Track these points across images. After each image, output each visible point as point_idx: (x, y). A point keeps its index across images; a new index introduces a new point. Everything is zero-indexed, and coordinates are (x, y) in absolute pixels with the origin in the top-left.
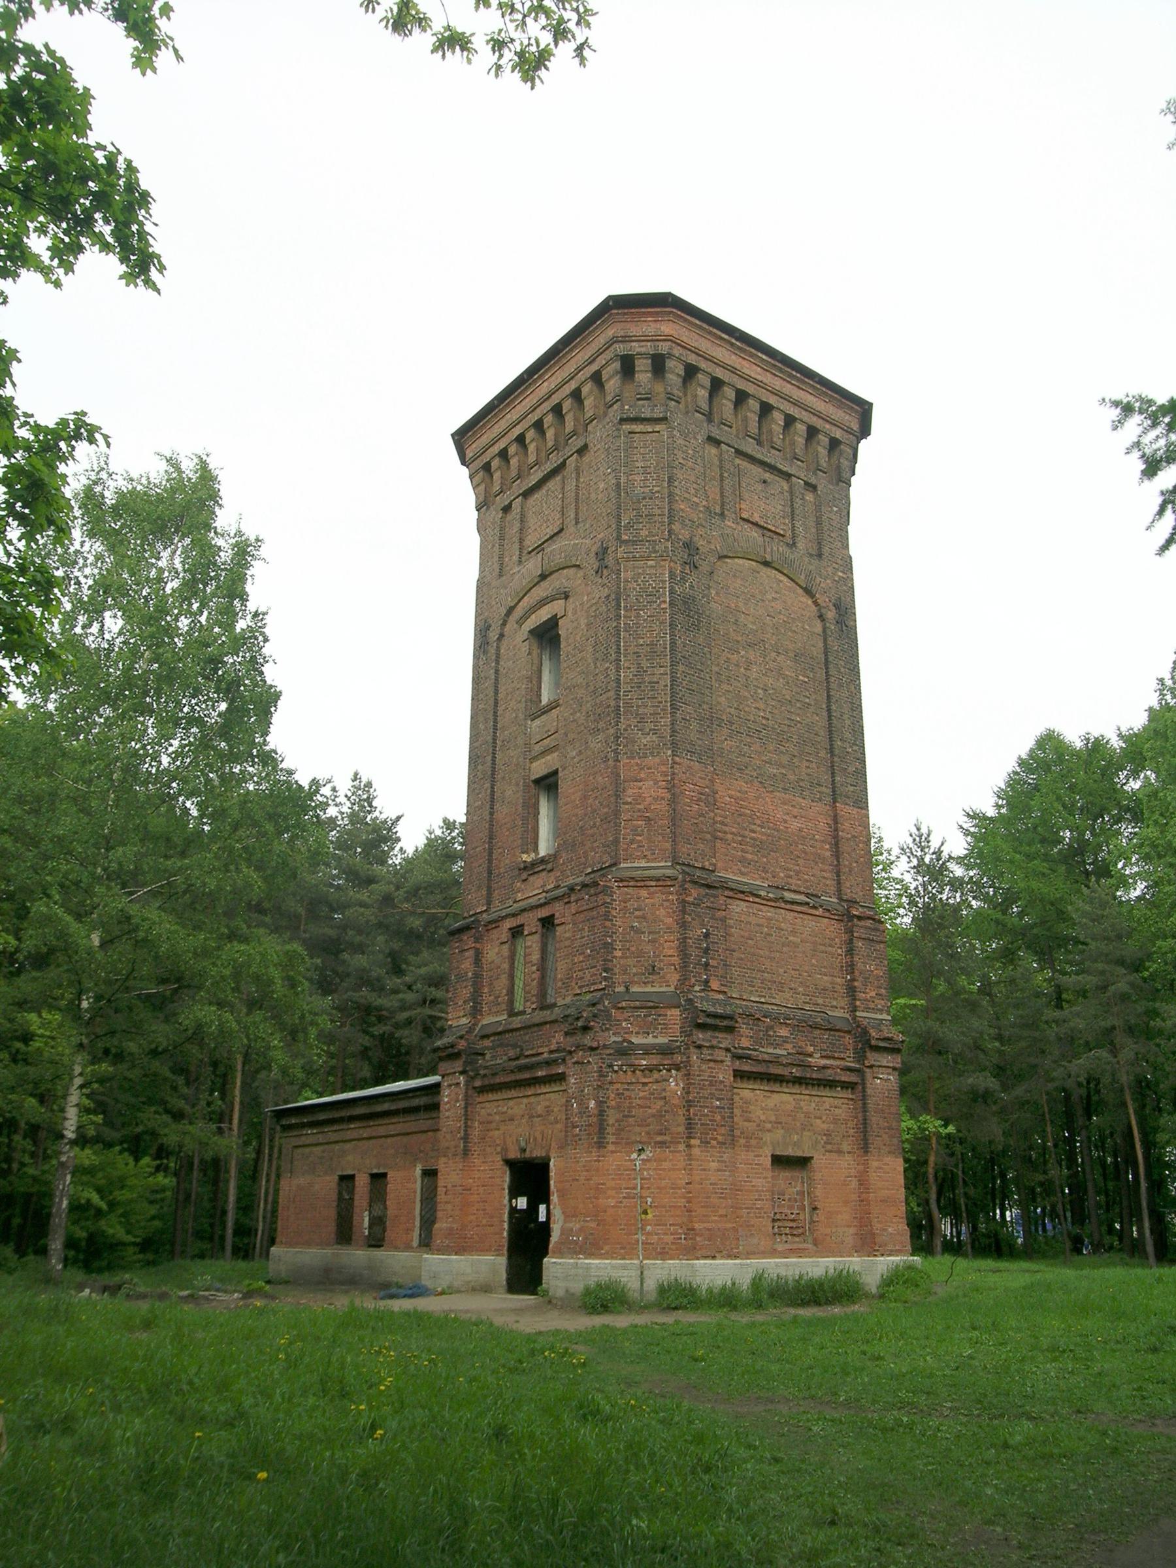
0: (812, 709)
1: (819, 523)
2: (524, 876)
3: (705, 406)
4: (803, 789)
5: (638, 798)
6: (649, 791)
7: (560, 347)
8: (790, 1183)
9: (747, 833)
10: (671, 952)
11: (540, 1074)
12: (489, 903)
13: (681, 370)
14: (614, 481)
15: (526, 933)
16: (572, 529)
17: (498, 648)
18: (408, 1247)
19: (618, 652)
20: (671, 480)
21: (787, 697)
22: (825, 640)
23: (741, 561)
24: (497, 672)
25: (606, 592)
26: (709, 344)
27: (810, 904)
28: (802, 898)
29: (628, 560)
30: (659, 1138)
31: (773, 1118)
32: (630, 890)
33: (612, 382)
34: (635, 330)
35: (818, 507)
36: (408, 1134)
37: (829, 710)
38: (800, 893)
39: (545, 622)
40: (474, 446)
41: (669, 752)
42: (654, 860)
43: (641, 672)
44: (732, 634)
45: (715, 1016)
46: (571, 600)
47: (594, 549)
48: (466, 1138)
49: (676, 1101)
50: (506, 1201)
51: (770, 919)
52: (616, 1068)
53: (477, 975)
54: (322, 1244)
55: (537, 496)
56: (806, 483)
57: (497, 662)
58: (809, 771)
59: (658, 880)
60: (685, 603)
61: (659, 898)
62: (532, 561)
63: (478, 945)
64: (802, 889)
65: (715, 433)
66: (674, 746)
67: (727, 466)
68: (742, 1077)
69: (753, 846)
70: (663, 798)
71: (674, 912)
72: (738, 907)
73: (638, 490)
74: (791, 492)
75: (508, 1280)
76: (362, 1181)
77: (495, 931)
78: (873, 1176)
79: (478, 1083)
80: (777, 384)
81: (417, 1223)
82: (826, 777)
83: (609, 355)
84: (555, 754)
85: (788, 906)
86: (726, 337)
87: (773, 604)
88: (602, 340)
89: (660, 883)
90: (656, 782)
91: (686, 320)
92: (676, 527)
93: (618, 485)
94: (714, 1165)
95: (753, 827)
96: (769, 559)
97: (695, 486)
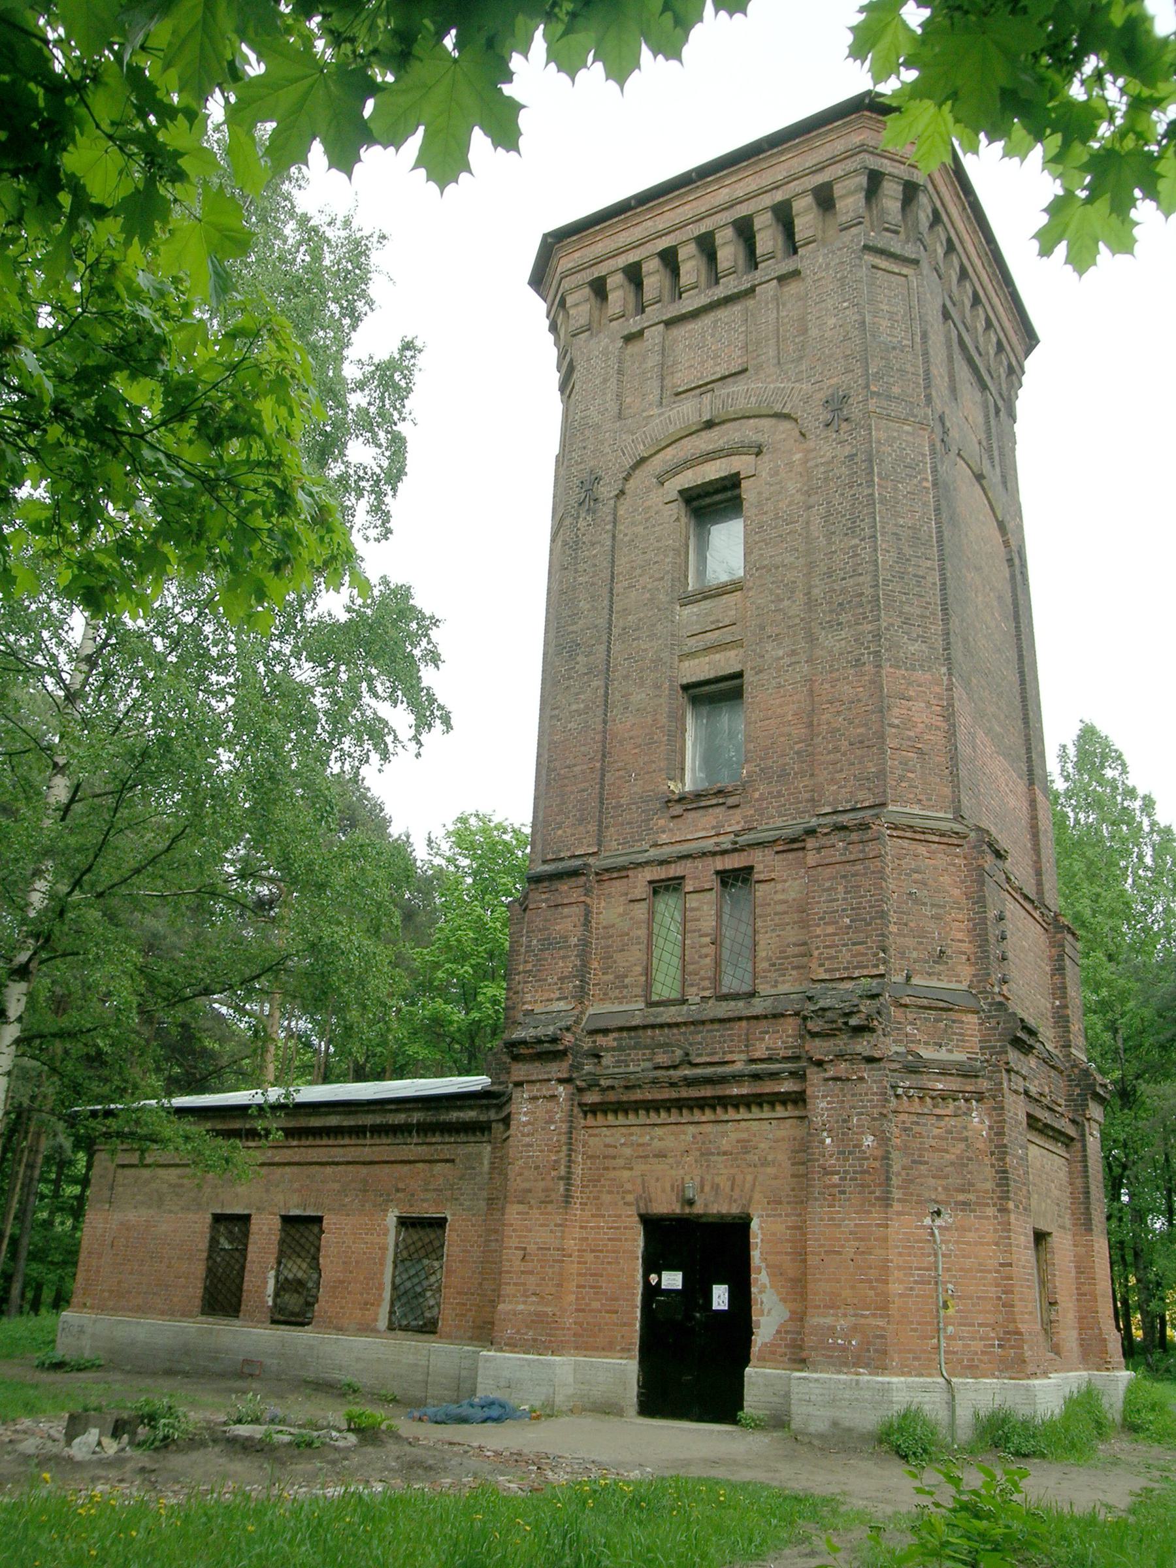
2: (677, 809)
7: (766, 146)
10: (960, 936)
11: (736, 1091)
15: (689, 888)
18: (366, 1329)
25: (847, 450)
30: (961, 1197)
32: (905, 843)
33: (850, 200)
36: (371, 1163)
39: (711, 482)
40: (577, 255)
41: (944, 670)
43: (902, 558)
46: (765, 458)
47: (821, 395)
48: (568, 1179)
49: (981, 1146)
50: (639, 1277)
52: (900, 1091)
53: (585, 943)
54: (169, 1312)
55: (691, 326)
61: (941, 860)
63: (588, 900)
70: (938, 728)
75: (640, 1395)
76: (265, 1233)
77: (617, 883)
79: (592, 1098)
81: (387, 1294)
83: (850, 165)
84: (732, 653)
88: (839, 146)
89: (945, 840)
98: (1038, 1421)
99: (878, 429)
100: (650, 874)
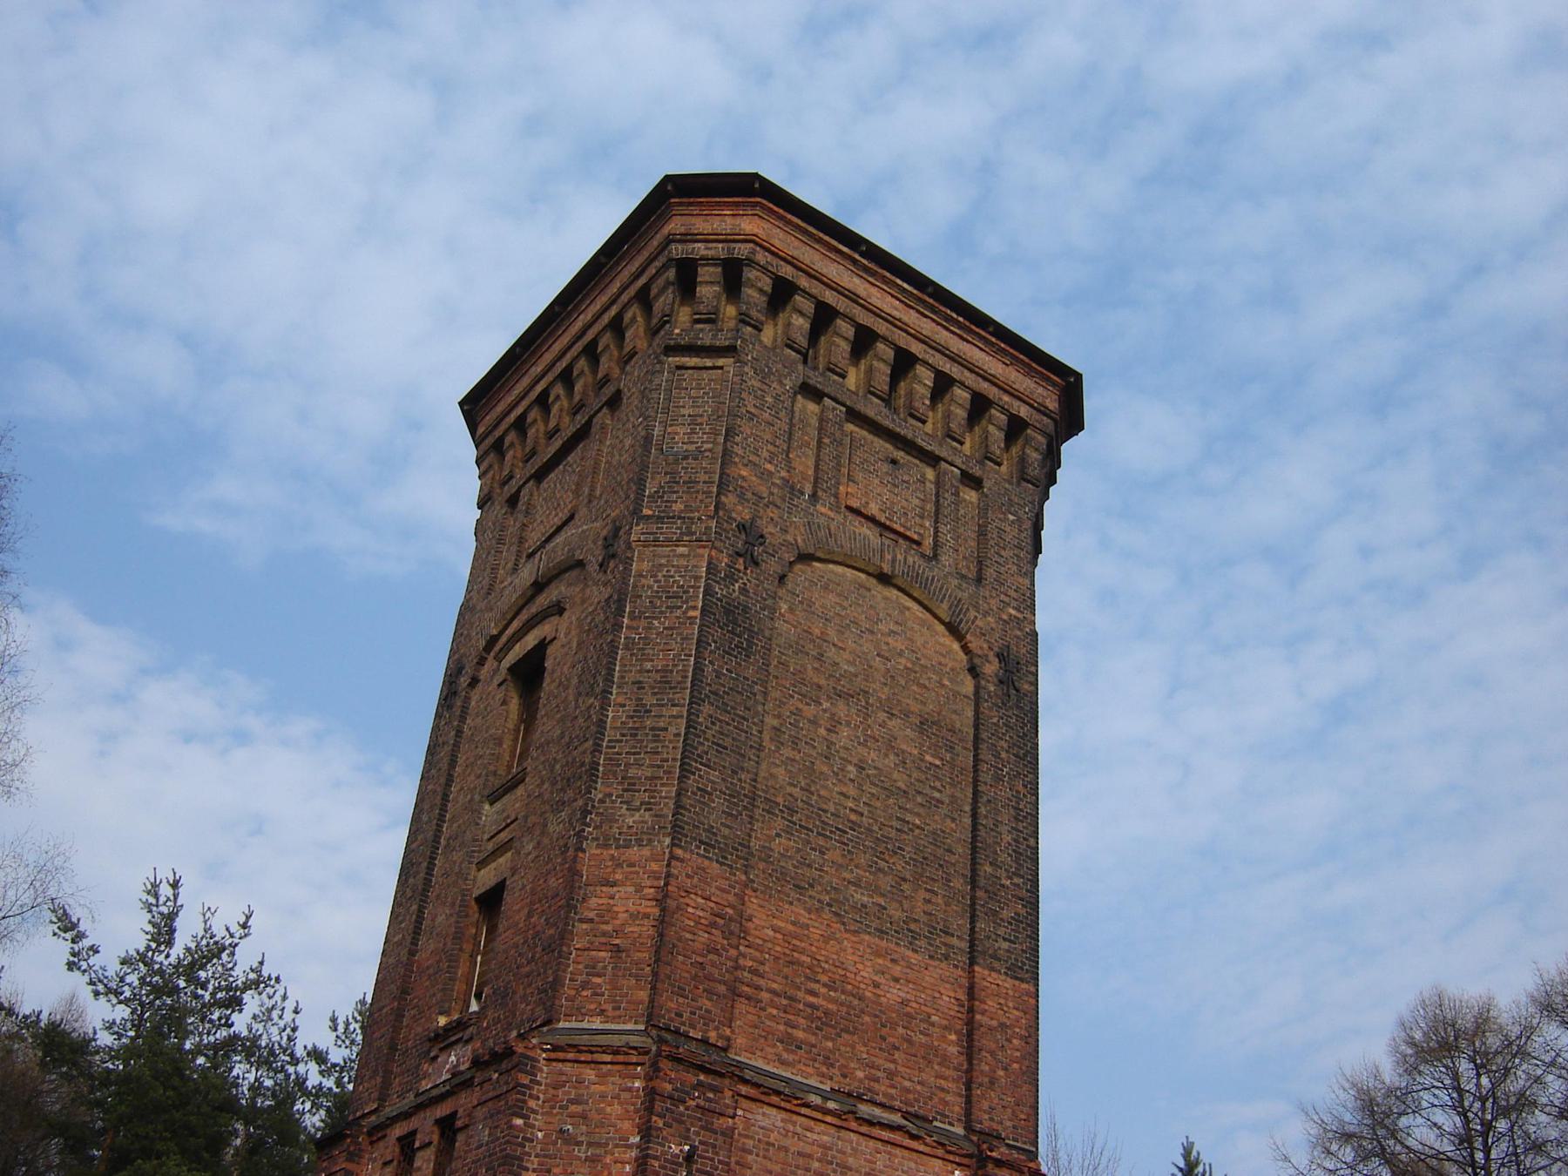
0: (944, 810)
1: (982, 533)
3: (803, 342)
4: (915, 936)
5: (606, 913)
6: (622, 902)
9: (800, 995)
12: (382, 1099)
13: (766, 283)
14: (643, 433)
15: (417, 1145)
16: (583, 511)
17: (467, 699)
19: (609, 679)
20: (730, 433)
21: (901, 784)
22: (977, 705)
23: (840, 569)
24: (459, 732)
26: (817, 257)
28: (897, 1118)
29: (646, 544)
32: (567, 1068)
34: (701, 225)
35: (983, 510)
37: (975, 815)
38: (891, 1109)
41: (668, 841)
42: (614, 1020)
43: (641, 711)
44: (810, 672)
46: (566, 615)
51: (824, 1147)
56: (964, 474)
57: (463, 719)
58: (929, 908)
59: (616, 1052)
60: (728, 612)
62: (529, 566)
64: (897, 1104)
65: (816, 380)
66: (677, 832)
67: (830, 428)
69: (810, 1018)
70: (646, 916)
71: (637, 1111)
72: (768, 1119)
73: (679, 447)
74: (938, 483)
80: (927, 327)
82: (960, 923)
85: (864, 1129)
86: (845, 249)
87: (890, 640)
89: (621, 1058)
90: (639, 888)
91: (781, 218)
92: (729, 500)
93: (648, 439)
95: (816, 986)
96: (887, 568)
97: (770, 447)
98: (74, 1035)
99: (641, 560)
100: (398, 1131)
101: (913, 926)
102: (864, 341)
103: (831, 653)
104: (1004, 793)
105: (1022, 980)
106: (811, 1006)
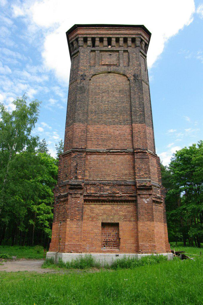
8: (111, 231)
27: (122, 152)
31: (103, 212)
38: (118, 149)
45: (74, 185)
56: (124, 51)
60: (80, 88)
68: (87, 202)
78: (140, 229)
85: (112, 154)
91: (82, 28)
94: (75, 226)
96: (109, 71)
101: (120, 122)
102: (101, 40)
103: (101, 87)
104: (137, 96)
105: (142, 123)
106: (102, 138)
